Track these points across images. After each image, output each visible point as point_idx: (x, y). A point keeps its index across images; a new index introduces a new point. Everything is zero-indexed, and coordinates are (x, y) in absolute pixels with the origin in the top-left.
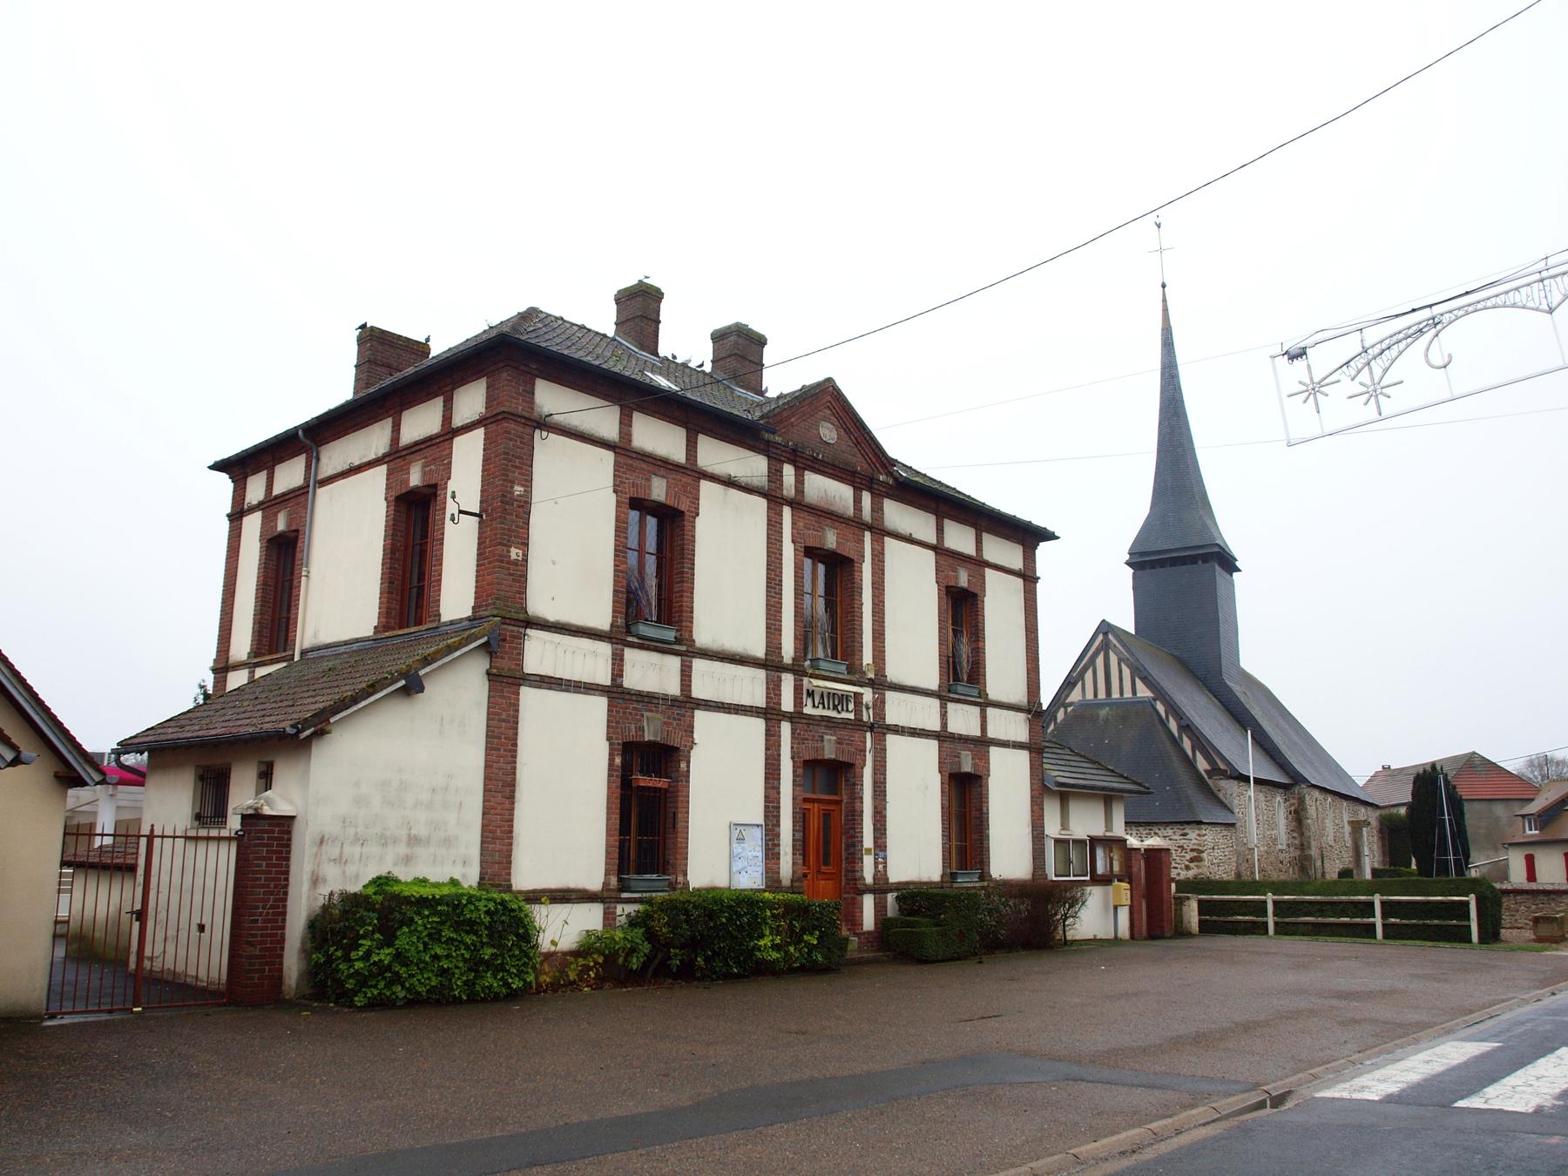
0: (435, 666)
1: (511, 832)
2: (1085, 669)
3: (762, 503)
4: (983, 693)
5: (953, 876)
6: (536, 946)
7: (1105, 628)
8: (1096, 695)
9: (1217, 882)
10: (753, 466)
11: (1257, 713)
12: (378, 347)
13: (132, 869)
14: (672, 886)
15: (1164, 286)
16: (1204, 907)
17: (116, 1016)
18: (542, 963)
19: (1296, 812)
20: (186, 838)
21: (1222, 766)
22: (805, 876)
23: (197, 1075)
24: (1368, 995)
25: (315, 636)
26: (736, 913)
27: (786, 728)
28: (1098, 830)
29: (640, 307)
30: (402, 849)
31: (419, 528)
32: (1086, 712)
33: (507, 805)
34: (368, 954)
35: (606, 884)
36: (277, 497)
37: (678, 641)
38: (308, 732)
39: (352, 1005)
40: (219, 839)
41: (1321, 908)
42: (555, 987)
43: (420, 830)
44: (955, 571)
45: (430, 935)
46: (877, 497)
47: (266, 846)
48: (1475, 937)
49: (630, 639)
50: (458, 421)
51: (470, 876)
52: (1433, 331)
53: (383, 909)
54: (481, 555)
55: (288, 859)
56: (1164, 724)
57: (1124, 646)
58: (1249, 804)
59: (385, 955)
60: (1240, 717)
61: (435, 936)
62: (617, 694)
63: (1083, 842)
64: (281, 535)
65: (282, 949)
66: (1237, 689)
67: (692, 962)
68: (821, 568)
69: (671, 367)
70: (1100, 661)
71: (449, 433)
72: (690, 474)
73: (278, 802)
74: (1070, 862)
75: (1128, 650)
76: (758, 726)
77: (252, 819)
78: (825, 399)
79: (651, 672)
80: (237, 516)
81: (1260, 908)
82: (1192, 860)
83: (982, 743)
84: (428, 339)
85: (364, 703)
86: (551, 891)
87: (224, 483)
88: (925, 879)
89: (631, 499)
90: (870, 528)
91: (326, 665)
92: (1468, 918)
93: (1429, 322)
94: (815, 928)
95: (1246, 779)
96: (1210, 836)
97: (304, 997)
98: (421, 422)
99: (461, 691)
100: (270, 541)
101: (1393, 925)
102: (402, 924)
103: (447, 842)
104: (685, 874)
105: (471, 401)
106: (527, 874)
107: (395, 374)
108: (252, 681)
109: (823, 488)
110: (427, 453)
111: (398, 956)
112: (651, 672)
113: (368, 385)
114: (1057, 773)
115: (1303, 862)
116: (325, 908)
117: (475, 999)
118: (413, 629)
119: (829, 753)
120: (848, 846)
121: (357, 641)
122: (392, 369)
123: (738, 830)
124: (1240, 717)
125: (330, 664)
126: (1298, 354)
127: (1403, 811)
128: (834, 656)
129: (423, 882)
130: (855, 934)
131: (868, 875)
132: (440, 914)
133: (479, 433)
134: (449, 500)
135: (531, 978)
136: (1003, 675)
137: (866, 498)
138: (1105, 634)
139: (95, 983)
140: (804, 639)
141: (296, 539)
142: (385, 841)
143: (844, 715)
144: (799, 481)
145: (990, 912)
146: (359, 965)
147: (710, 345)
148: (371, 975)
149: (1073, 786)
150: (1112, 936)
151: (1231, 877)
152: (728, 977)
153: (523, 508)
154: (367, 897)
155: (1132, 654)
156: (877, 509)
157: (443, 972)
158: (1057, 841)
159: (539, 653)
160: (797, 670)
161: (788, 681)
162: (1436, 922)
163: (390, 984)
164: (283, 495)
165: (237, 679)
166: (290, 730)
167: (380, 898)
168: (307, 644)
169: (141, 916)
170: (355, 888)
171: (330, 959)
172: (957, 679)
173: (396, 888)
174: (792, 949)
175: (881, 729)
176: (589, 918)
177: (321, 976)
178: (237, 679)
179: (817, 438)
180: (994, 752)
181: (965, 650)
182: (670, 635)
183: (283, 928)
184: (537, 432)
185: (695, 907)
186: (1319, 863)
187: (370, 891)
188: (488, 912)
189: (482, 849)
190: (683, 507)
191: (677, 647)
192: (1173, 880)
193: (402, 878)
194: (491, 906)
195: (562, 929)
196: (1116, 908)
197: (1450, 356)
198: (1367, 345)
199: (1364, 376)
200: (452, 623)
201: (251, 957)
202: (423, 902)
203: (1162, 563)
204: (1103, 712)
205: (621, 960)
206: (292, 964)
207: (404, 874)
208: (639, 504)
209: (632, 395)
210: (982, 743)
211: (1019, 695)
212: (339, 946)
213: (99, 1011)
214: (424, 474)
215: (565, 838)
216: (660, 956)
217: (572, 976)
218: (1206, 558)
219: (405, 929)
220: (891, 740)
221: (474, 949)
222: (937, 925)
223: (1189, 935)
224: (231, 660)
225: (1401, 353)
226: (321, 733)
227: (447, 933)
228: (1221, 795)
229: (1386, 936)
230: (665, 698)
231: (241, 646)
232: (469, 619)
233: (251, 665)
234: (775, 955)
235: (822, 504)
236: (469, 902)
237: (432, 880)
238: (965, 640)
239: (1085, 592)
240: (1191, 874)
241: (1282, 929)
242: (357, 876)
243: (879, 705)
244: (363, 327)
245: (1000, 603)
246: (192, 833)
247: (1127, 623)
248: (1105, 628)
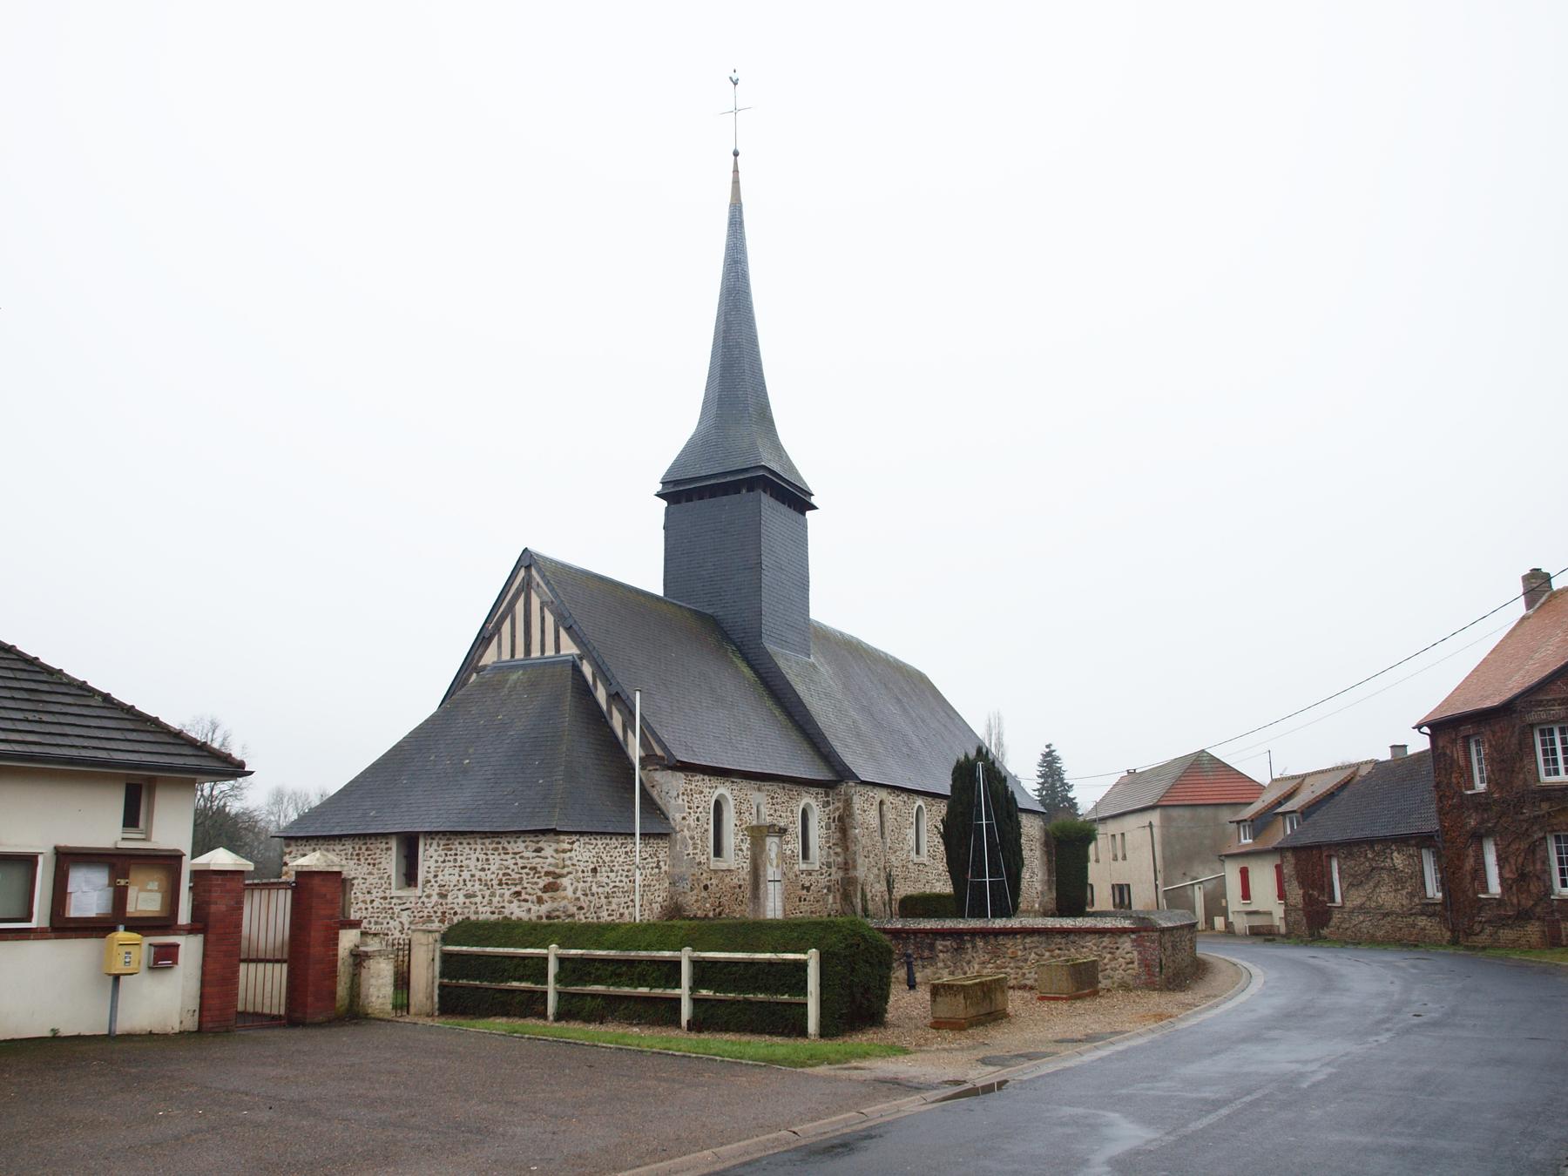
8: (513, 655)
15: (736, 154)
19: (841, 818)
21: (659, 752)
48: (813, 1024)
57: (548, 583)
82: (546, 889)
92: (803, 990)
101: (706, 1000)
115: (847, 887)
138: (528, 568)
162: (761, 996)
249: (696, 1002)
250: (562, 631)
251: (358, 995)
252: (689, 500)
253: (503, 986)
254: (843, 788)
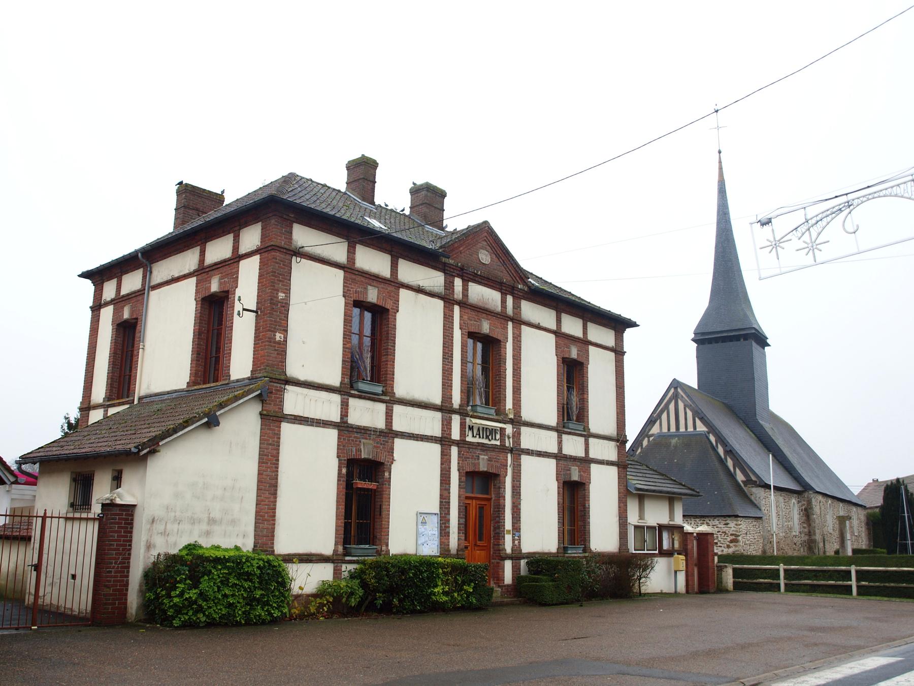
0: (226, 409)
1: (274, 516)
2: (662, 412)
3: (440, 304)
4: (586, 428)
5: (565, 549)
6: (290, 590)
7: (675, 384)
8: (669, 429)
9: (748, 556)
10: (434, 279)
11: (780, 442)
12: (191, 198)
13: (27, 539)
14: (379, 553)
15: (720, 152)
16: (736, 573)
17: (22, 632)
18: (293, 601)
19: (806, 510)
20: (67, 519)
21: (754, 478)
22: (466, 547)
23: (78, 664)
24: (823, 629)
25: (148, 388)
26: (419, 570)
27: (454, 451)
28: (665, 520)
29: (363, 172)
30: (204, 527)
31: (216, 319)
32: (662, 441)
33: (272, 499)
34: (181, 595)
35: (335, 551)
36: (123, 296)
37: (384, 393)
38: (145, 451)
39: (171, 626)
40: (87, 519)
41: (816, 574)
42: (301, 617)
43: (216, 514)
44: (568, 347)
45: (221, 582)
46: (517, 299)
47: (118, 523)
49: (353, 392)
50: (243, 250)
51: (247, 545)
52: (848, 210)
53: (192, 565)
54: (257, 337)
55: (131, 532)
56: (715, 449)
57: (688, 396)
58: (771, 503)
59: (193, 594)
60: (768, 444)
61: (225, 582)
62: (343, 427)
63: (653, 528)
64: (126, 321)
65: (127, 590)
66: (767, 426)
67: (391, 602)
68: (479, 346)
69: (384, 212)
70: (672, 407)
71: (238, 257)
72: (394, 284)
73: (125, 496)
74: (645, 541)
75: (691, 399)
76: (436, 448)
77: (108, 506)
78: (483, 234)
79: (366, 414)
80: (96, 308)
81: (775, 574)
82: (731, 541)
83: (585, 462)
84: (223, 192)
85: (181, 433)
86: (299, 555)
87: (88, 286)
88: (546, 551)
89: (354, 301)
90: (512, 319)
91: (156, 407)
93: (846, 205)
94: (471, 581)
95: (768, 487)
96: (744, 525)
97: (140, 621)
98: (219, 250)
99: (243, 425)
100: (118, 325)
101: (864, 586)
102: (204, 574)
103: (233, 522)
104: (387, 545)
105: (251, 237)
106: (284, 544)
107: (202, 218)
108: (106, 417)
109: (480, 293)
110: (224, 269)
111: (201, 594)
112: (366, 414)
113: (184, 222)
114: (636, 482)
115: (810, 544)
116: (154, 564)
117: (251, 623)
118: (212, 385)
119: (483, 467)
120: (495, 528)
121: (176, 391)
122: (200, 212)
123: (422, 517)
124: (768, 444)
125: (159, 407)
126: (769, 222)
127: (877, 510)
128: (487, 403)
129: (217, 548)
130: (499, 586)
131: (508, 547)
132: (228, 568)
133: (256, 259)
134: (237, 301)
135: (286, 610)
136: (600, 417)
137: (510, 300)
138: (676, 388)
139: (8, 613)
140: (467, 392)
141: (136, 323)
142: (193, 521)
143: (493, 442)
144: (465, 289)
145: (589, 573)
146: (176, 600)
147: (408, 197)
148: (184, 606)
149: (647, 490)
150: (673, 591)
151: (759, 553)
152: (414, 612)
153: (285, 307)
154: (182, 557)
155: (694, 402)
156: (517, 307)
157: (230, 605)
158: (636, 527)
159: (294, 401)
160: (462, 412)
161: (456, 420)
162: (892, 584)
163: (196, 612)
164: (128, 295)
165: (96, 416)
166: (134, 450)
167: (190, 558)
168: (143, 393)
169: (37, 568)
170: (174, 551)
171: (157, 597)
172: (569, 419)
173: (200, 552)
174: (456, 595)
175: (518, 452)
176: (323, 573)
177: (152, 607)
178: (96, 416)
179: (475, 262)
180: (594, 467)
181: (575, 400)
182: (379, 389)
183: (128, 576)
184: (294, 258)
185: (393, 566)
186: (821, 545)
187: (184, 553)
188: (259, 568)
189: (256, 527)
190: (388, 306)
191: (383, 397)
192: (716, 554)
193: (204, 545)
194: (261, 563)
195: (306, 580)
196: (676, 572)
197: (858, 226)
198: (808, 217)
199: (806, 237)
200: (238, 381)
201: (106, 595)
202: (217, 560)
203: (717, 340)
204: (674, 441)
205: (344, 600)
206: (133, 600)
207: (205, 543)
208: (360, 304)
209: (354, 234)
210: (585, 462)
211: (610, 429)
212: (164, 587)
213: (10, 628)
214: (220, 284)
215: (309, 521)
216: (370, 598)
217: (313, 610)
218: (746, 337)
219: (206, 578)
220: (525, 459)
221: (250, 591)
222: (553, 581)
223: (727, 591)
224: (92, 403)
225: (828, 223)
226: (153, 452)
227: (233, 580)
228: (752, 498)
229: (859, 594)
230: (375, 430)
231: (99, 393)
232: (248, 379)
233: (105, 406)
234: (445, 598)
235: (480, 304)
236: (247, 561)
237: (223, 547)
238: (575, 393)
239: (659, 362)
240: (730, 551)
241: (790, 588)
242: (175, 544)
243: (517, 436)
244: (181, 183)
245: (599, 368)
246: (70, 515)
247: (692, 381)
248: (675, 384)
249: (858, 587)
250: (697, 420)
251: (721, 582)
252: (717, 342)
253: (755, 581)
254: (806, 495)
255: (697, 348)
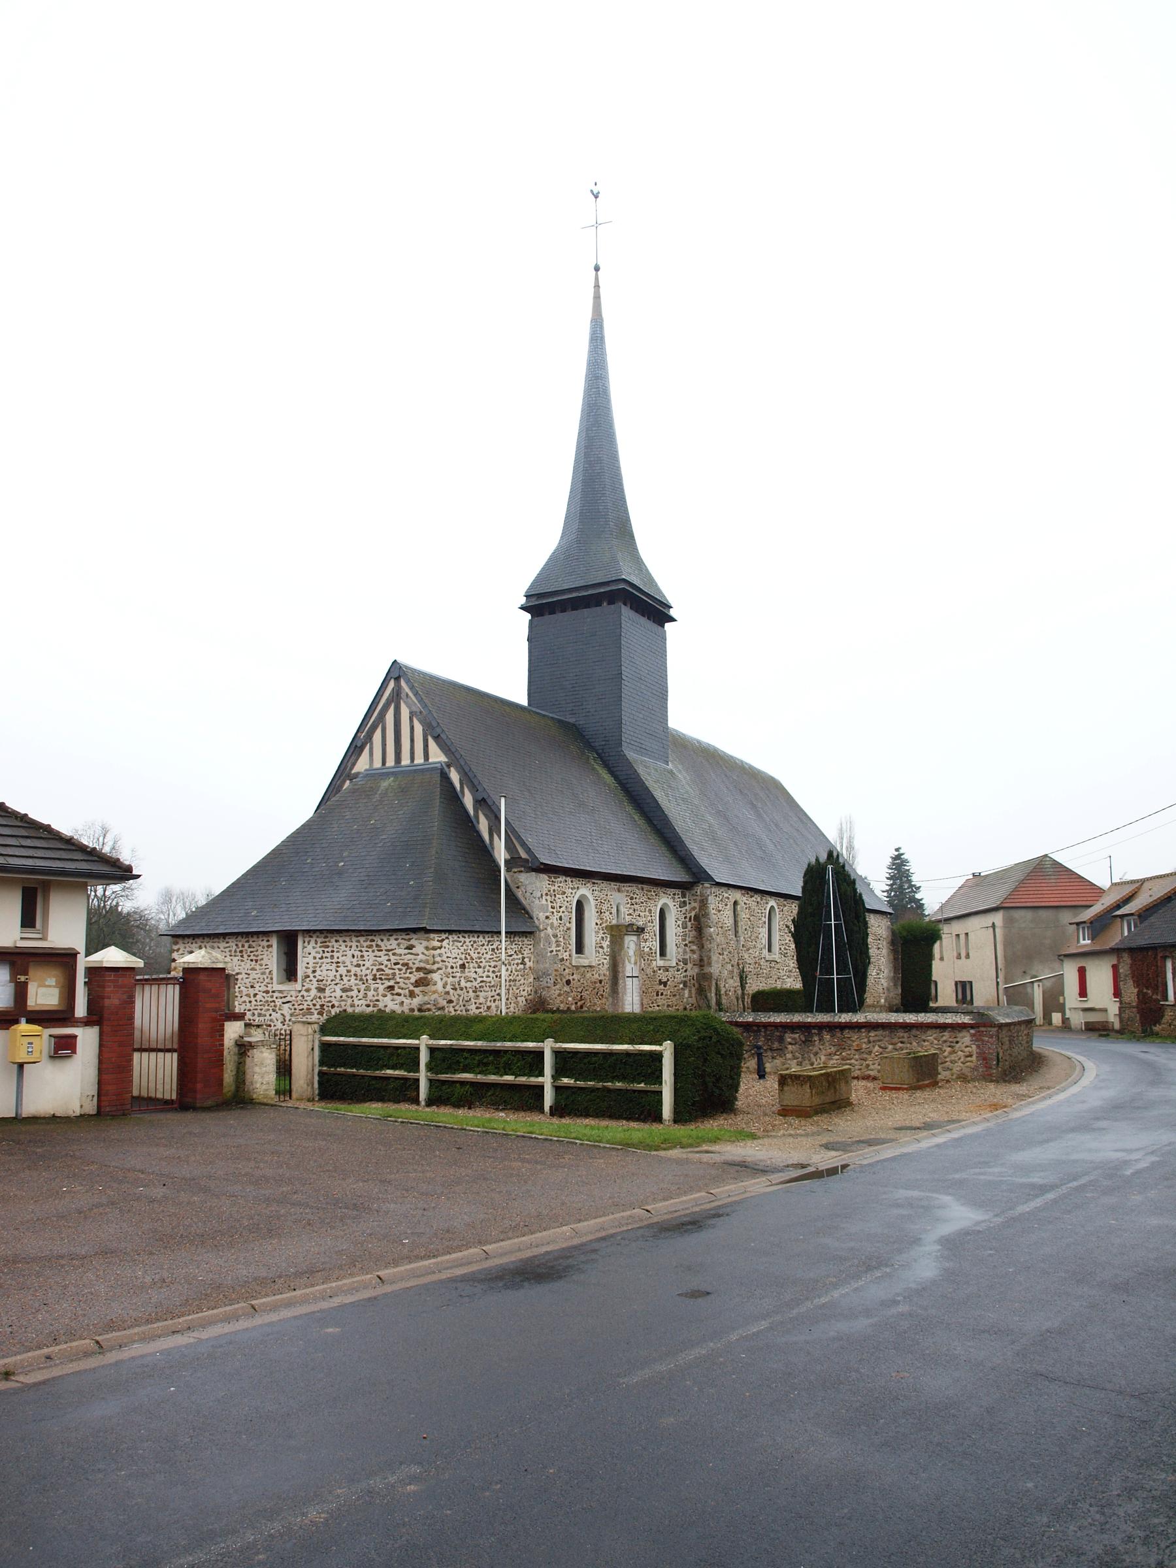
8: (384, 763)
15: (597, 269)
19: (697, 918)
21: (524, 855)
48: (667, 1110)
57: (416, 694)
82: (417, 984)
92: (658, 1079)
115: (702, 982)
138: (397, 679)
162: (619, 1085)
241: (441, 1096)
253: (378, 1073)
254: (698, 889)
255: (531, 622)
